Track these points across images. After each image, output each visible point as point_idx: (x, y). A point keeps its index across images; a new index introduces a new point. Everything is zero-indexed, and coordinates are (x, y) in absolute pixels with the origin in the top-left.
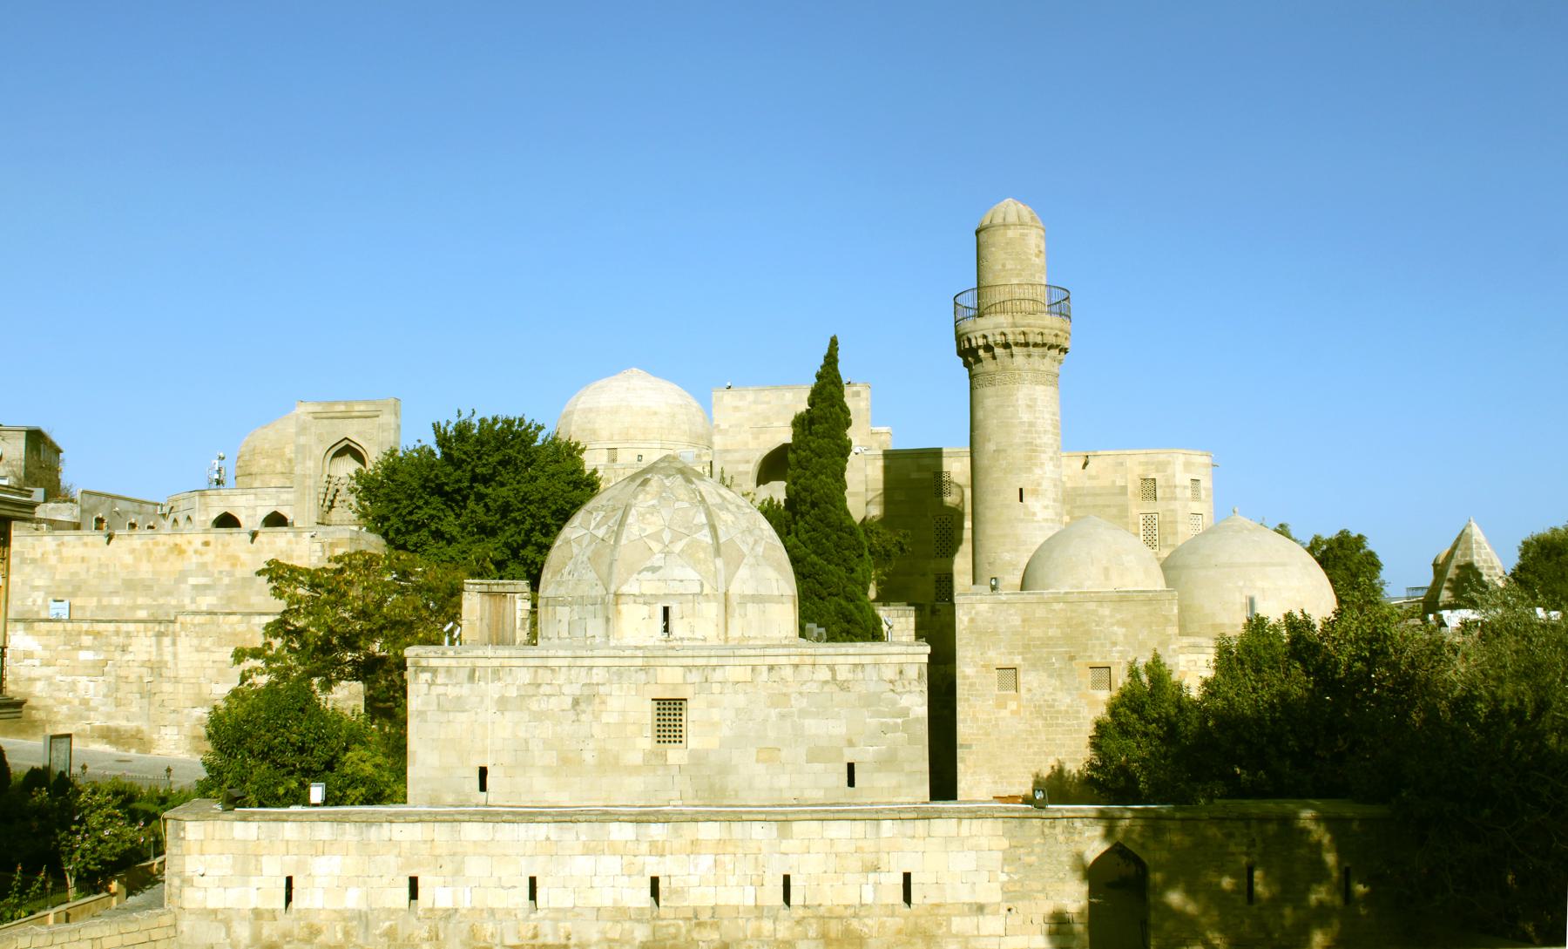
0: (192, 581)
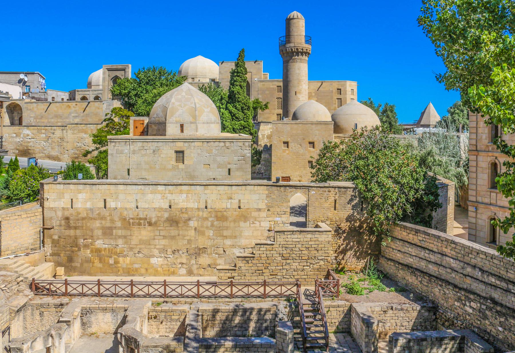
0: (73, 115)
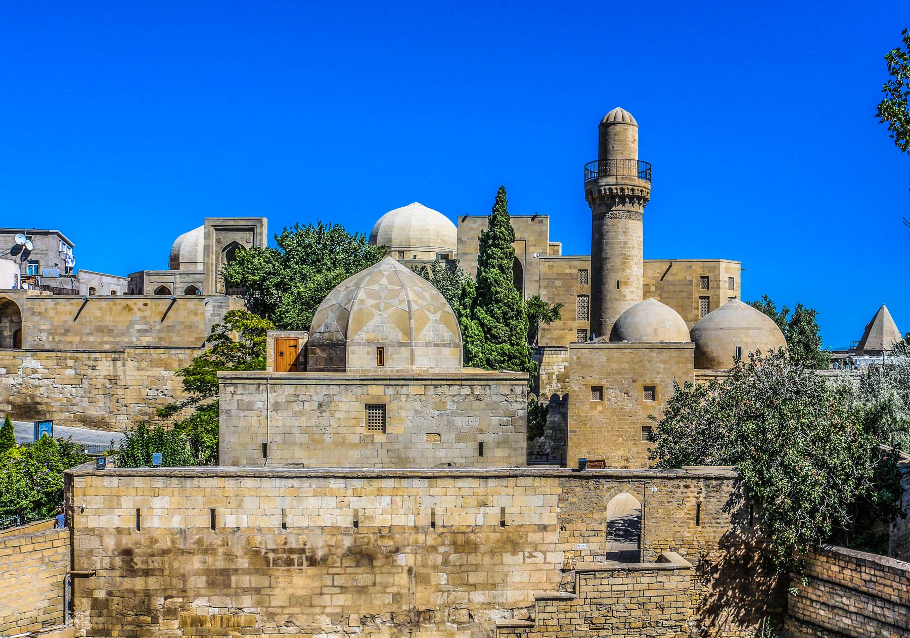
0: (137, 327)
